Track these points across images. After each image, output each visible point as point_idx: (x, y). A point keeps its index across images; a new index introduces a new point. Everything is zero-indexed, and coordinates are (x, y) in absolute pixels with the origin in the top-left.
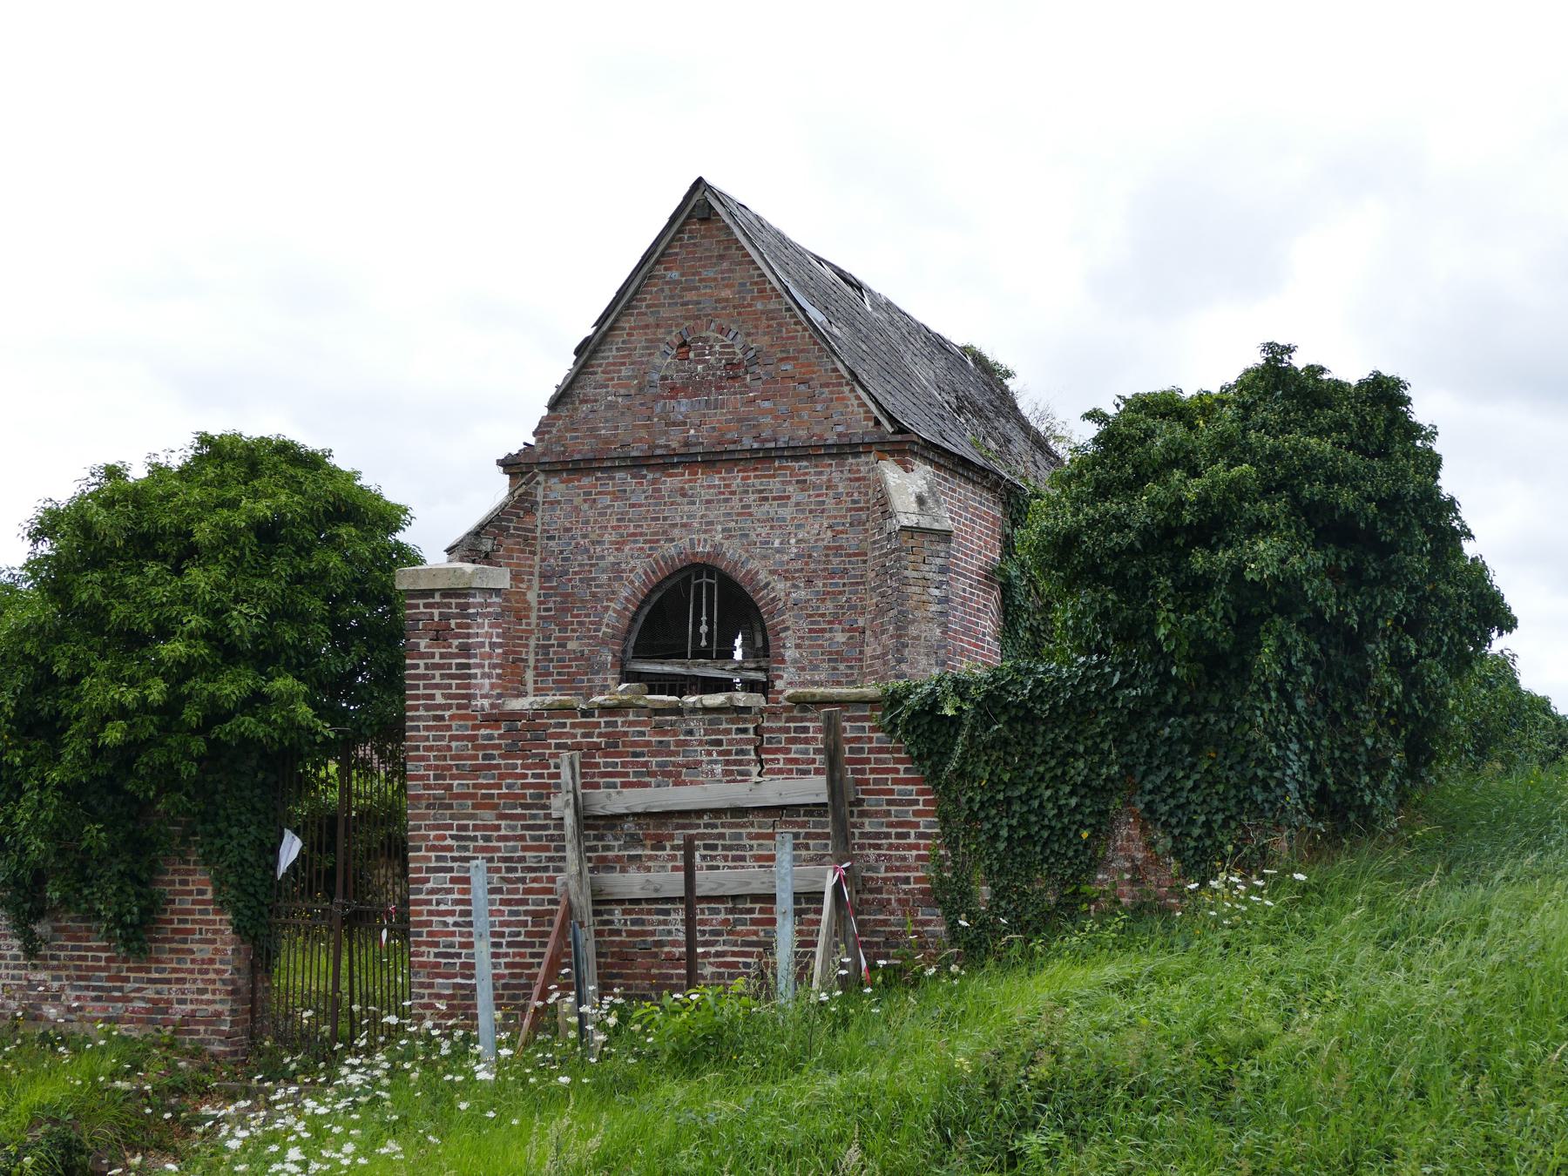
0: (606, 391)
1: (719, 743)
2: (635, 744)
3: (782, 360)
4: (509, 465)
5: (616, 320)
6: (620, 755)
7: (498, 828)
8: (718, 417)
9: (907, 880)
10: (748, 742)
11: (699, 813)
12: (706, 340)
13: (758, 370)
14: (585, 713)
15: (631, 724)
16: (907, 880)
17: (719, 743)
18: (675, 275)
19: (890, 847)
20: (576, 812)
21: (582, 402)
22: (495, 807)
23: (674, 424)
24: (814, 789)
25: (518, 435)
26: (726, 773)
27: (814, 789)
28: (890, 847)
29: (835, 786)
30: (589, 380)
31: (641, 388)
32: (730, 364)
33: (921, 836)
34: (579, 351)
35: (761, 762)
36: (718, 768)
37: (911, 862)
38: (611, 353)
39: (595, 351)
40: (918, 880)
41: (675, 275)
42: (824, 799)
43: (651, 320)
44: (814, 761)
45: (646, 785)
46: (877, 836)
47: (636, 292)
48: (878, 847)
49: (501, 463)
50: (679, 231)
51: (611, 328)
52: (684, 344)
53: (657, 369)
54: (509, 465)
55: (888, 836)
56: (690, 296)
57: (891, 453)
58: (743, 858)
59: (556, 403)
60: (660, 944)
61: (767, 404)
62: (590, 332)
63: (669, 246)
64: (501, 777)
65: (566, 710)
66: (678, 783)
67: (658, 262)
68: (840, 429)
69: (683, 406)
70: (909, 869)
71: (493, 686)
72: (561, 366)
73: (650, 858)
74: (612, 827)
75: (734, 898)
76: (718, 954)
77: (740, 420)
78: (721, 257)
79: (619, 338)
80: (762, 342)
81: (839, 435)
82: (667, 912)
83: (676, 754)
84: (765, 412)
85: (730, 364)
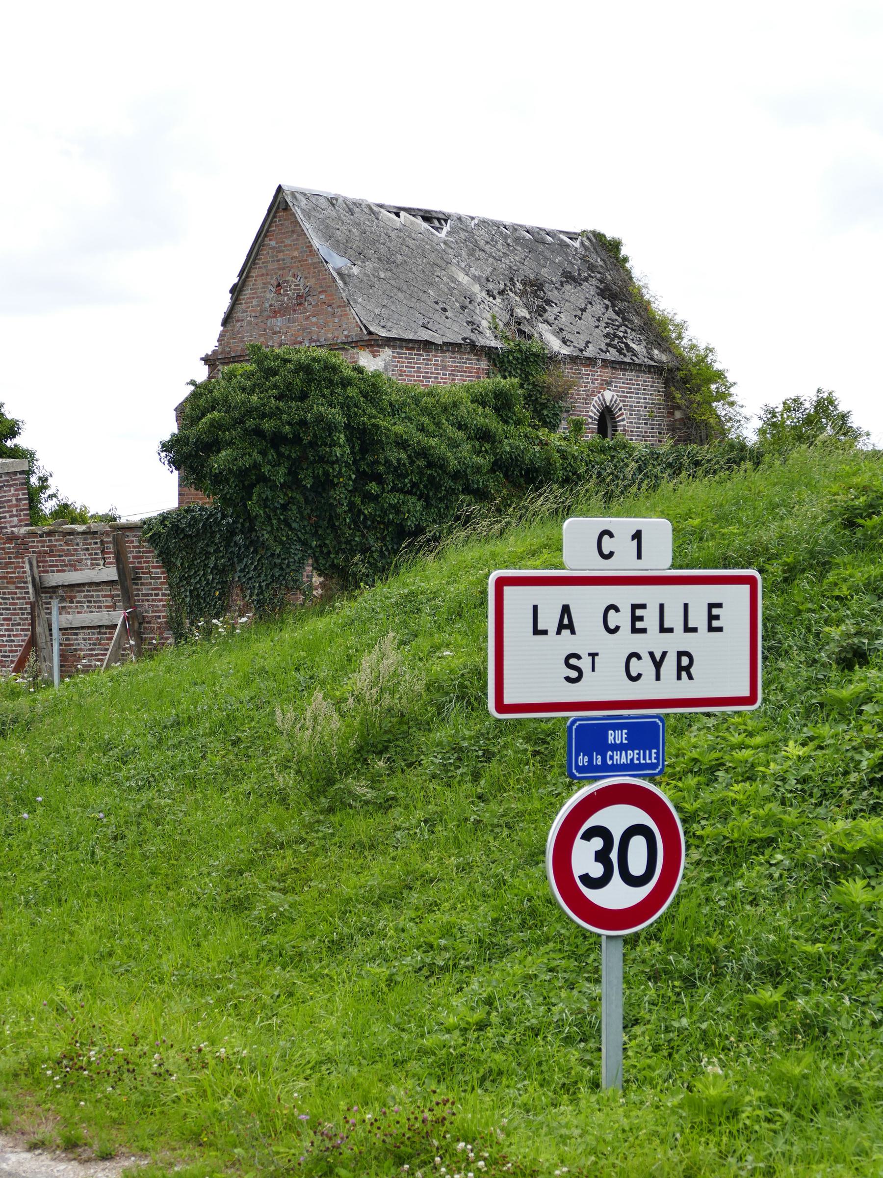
0: (244, 314)
1: (87, 549)
2: (59, 551)
3: (320, 292)
4: (207, 360)
5: (249, 272)
6: (54, 556)
7: (16, 593)
8: (294, 327)
9: (159, 617)
10: (98, 548)
11: (84, 585)
12: (287, 282)
13: (309, 298)
14: (41, 536)
15: (57, 540)
16: (159, 617)
17: (87, 549)
18: (273, 243)
19: (153, 600)
20: (34, 585)
21: (238, 321)
22: (14, 583)
23: (275, 333)
24: (110, 573)
25: (210, 345)
26: (92, 564)
27: (110, 573)
28: (153, 600)
29: (120, 572)
30: (239, 308)
31: (261, 312)
32: (299, 296)
33: (164, 595)
34: (232, 291)
35: (104, 559)
36: (89, 562)
37: (160, 608)
38: (248, 292)
39: (241, 291)
40: (164, 617)
41: (273, 243)
42: (116, 578)
43: (264, 271)
44: (134, 557)
45: (64, 571)
46: (147, 595)
47: (257, 254)
48: (148, 600)
49: (202, 359)
50: (274, 217)
51: (247, 277)
52: (279, 285)
53: (268, 300)
54: (207, 360)
55: (151, 595)
56: (281, 256)
57: (367, 346)
58: (100, 607)
59: (225, 323)
60: (76, 650)
61: (314, 320)
62: (236, 280)
63: (270, 226)
64: (16, 568)
65: (33, 534)
66: (76, 570)
67: (265, 236)
68: (346, 333)
69: (279, 322)
70: (160, 611)
71: (20, 521)
72: (226, 301)
73: (70, 607)
74: (54, 592)
75: (99, 627)
76: (97, 655)
77: (304, 329)
78: (293, 232)
79: (251, 282)
80: (311, 282)
81: (346, 336)
82: (77, 634)
83: (73, 555)
84: (313, 324)
85: (299, 296)
